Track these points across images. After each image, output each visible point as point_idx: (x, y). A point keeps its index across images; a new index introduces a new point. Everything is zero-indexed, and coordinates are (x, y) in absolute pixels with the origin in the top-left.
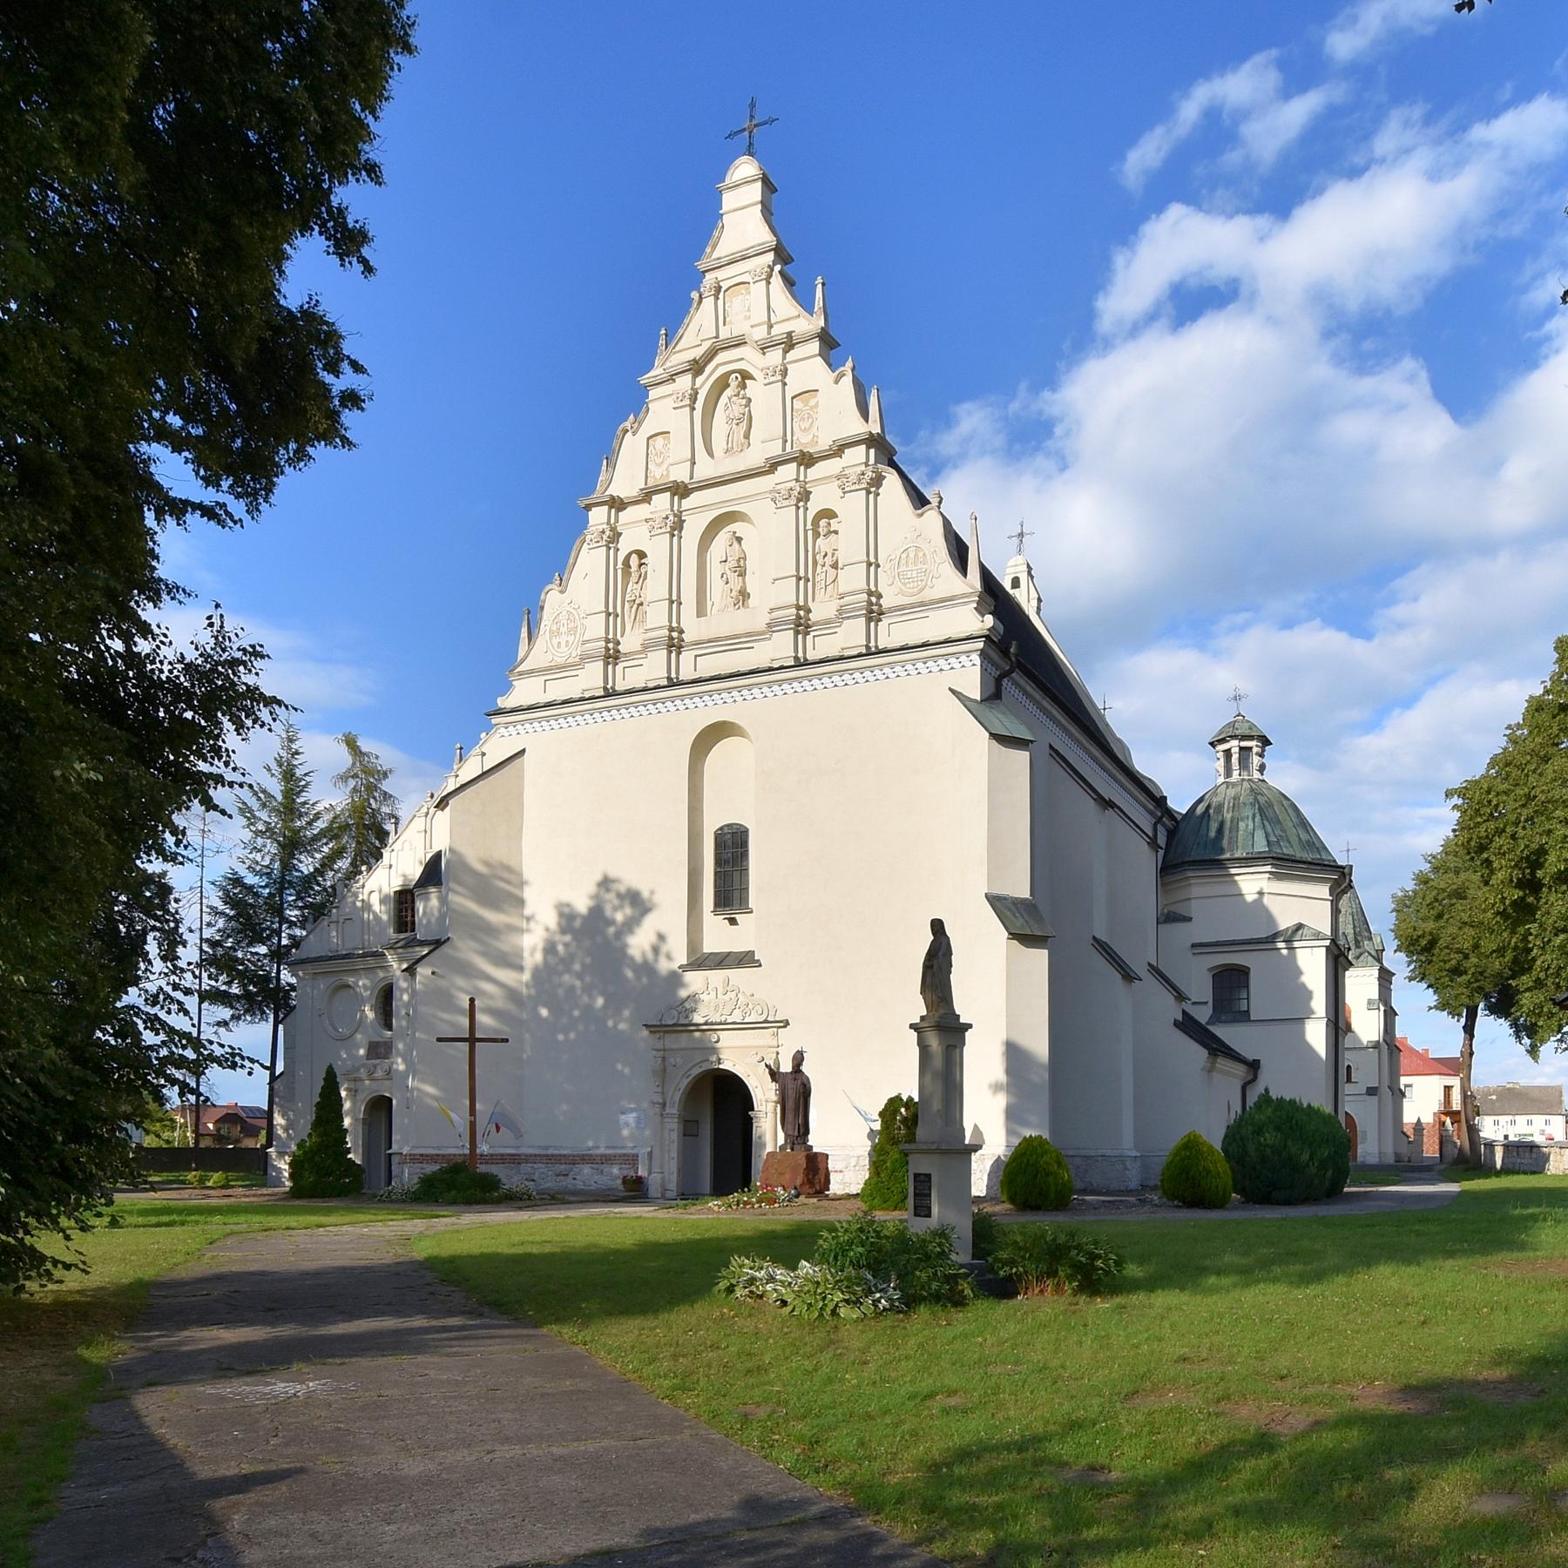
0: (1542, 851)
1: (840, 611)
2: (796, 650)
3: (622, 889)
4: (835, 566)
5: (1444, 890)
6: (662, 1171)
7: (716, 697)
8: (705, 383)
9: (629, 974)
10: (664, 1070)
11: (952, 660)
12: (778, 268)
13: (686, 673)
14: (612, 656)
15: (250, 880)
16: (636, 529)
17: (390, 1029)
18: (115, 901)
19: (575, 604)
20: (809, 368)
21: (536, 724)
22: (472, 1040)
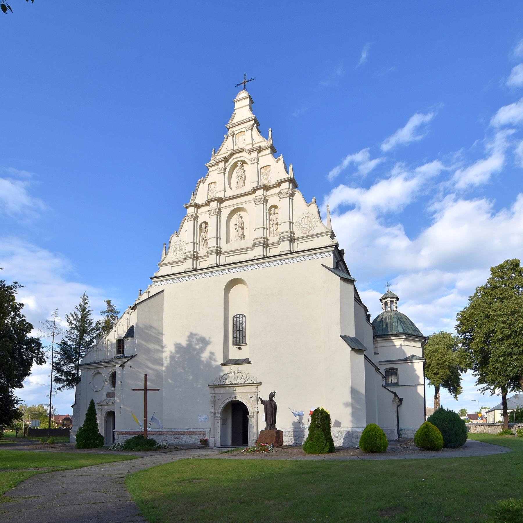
0: (493, 332)
1: (280, 238)
2: (263, 253)
3: (198, 337)
4: (277, 224)
5: (431, 350)
6: (215, 438)
7: (234, 270)
8: (229, 165)
9: (202, 367)
10: (215, 401)
11: (322, 254)
12: (255, 125)
13: (223, 262)
14: (196, 257)
15: (69, 343)
16: (204, 215)
17: (115, 388)
18: (22, 348)
19: (183, 239)
20: (267, 158)
21: (168, 281)
22: (146, 390)
